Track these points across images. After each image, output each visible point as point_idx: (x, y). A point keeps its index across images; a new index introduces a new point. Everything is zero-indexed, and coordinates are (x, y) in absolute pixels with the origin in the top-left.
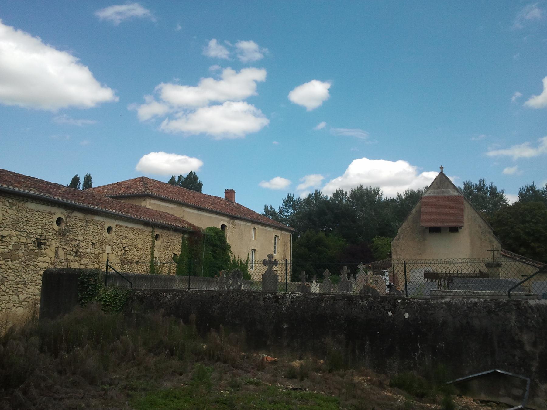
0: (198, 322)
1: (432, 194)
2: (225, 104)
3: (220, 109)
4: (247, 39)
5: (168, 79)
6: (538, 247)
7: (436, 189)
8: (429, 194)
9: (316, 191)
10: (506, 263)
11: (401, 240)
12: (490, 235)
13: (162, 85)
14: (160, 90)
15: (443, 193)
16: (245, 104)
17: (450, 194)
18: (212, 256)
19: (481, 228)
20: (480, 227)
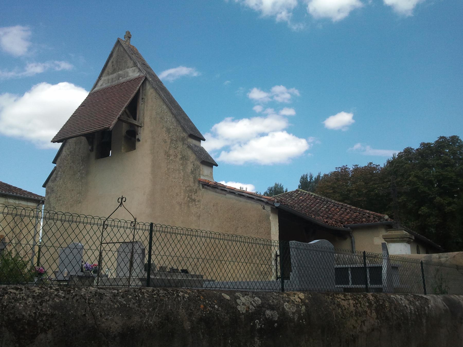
0: (24, 320)
1: (105, 86)
2: (270, 135)
3: (265, 138)
4: (279, 84)
5: (219, 119)
6: (449, 204)
7: (111, 74)
8: (101, 85)
9: (276, 184)
10: (196, 237)
11: (58, 179)
12: (183, 144)
13: (216, 126)
14: (216, 129)
15: (119, 79)
16: (285, 132)
17: (128, 78)
18: (288, 278)
19: (169, 133)
20: (168, 130)
